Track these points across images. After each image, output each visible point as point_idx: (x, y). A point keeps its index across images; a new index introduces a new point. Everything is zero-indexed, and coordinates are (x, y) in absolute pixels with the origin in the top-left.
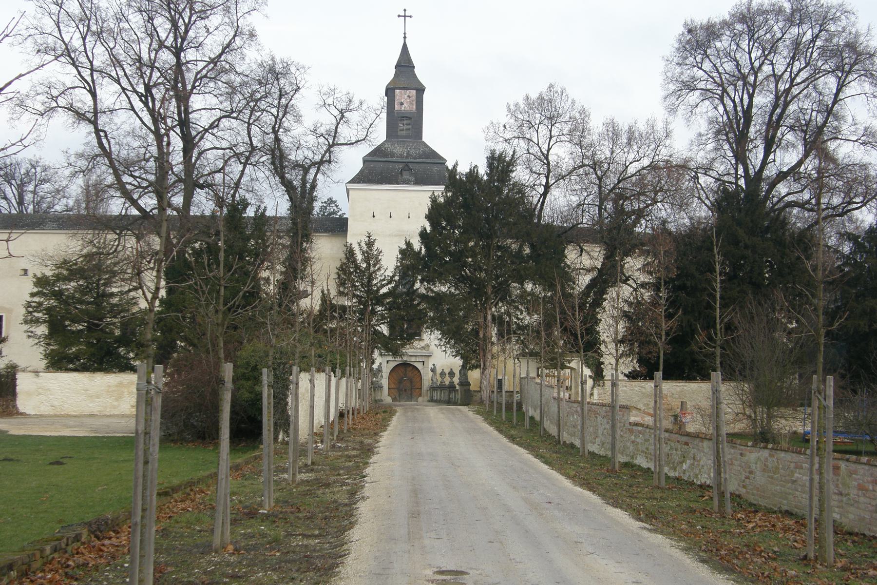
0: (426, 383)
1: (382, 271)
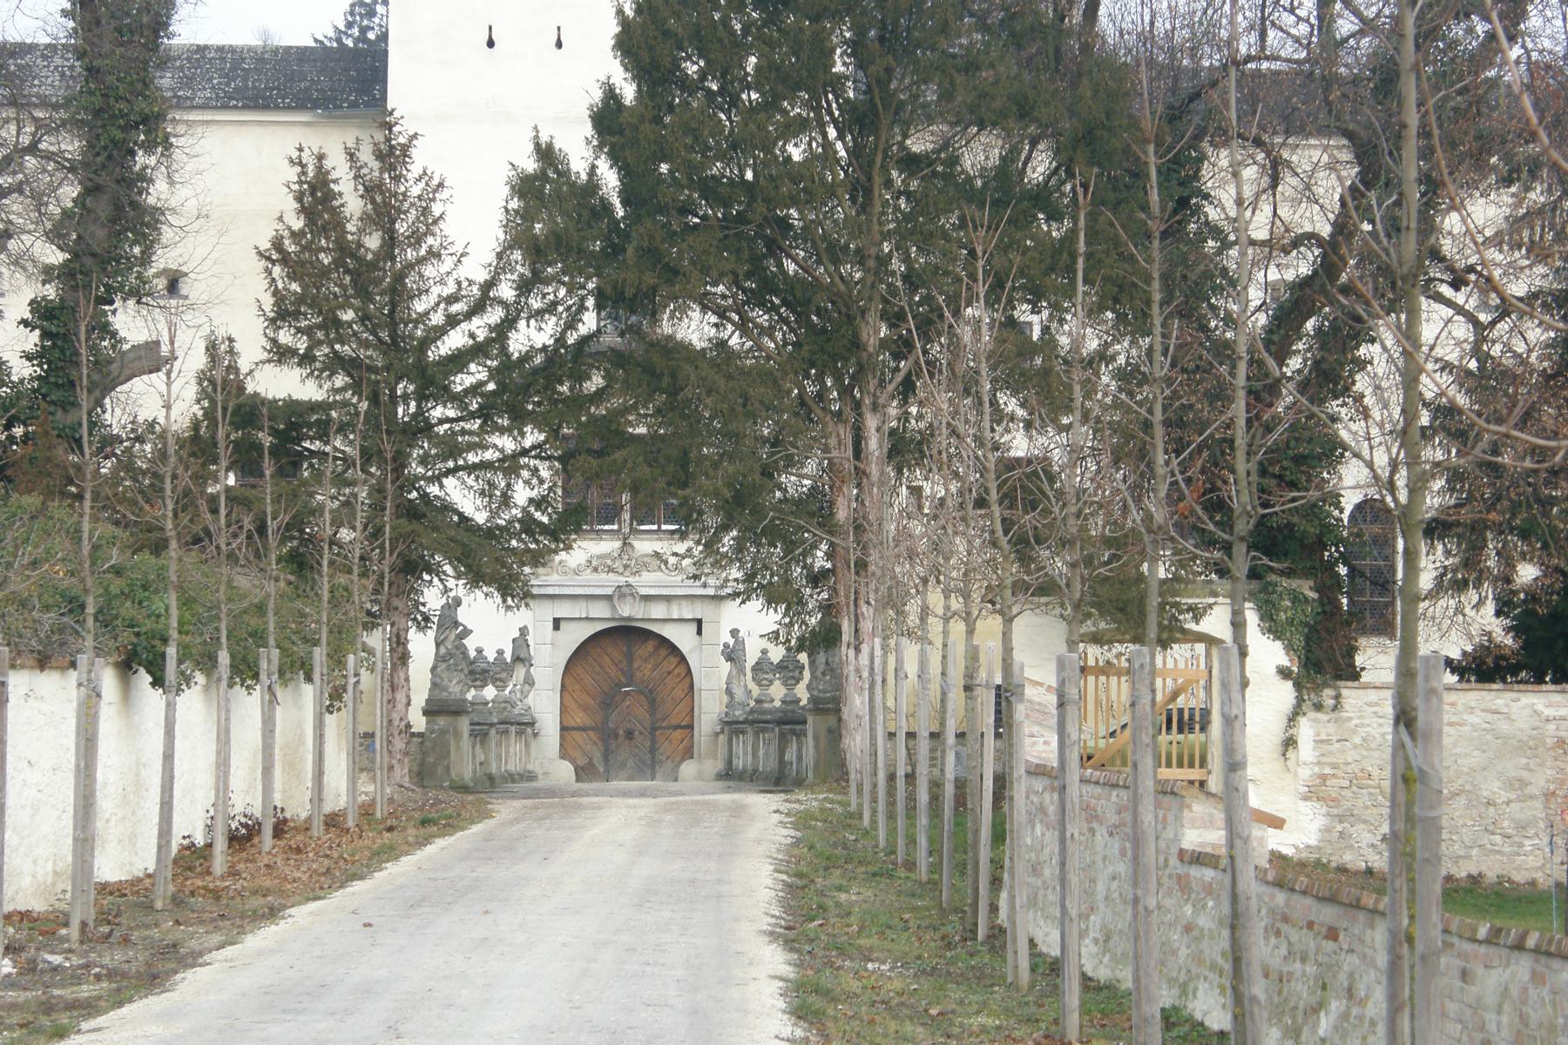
0: (710, 708)
1: (448, 263)
